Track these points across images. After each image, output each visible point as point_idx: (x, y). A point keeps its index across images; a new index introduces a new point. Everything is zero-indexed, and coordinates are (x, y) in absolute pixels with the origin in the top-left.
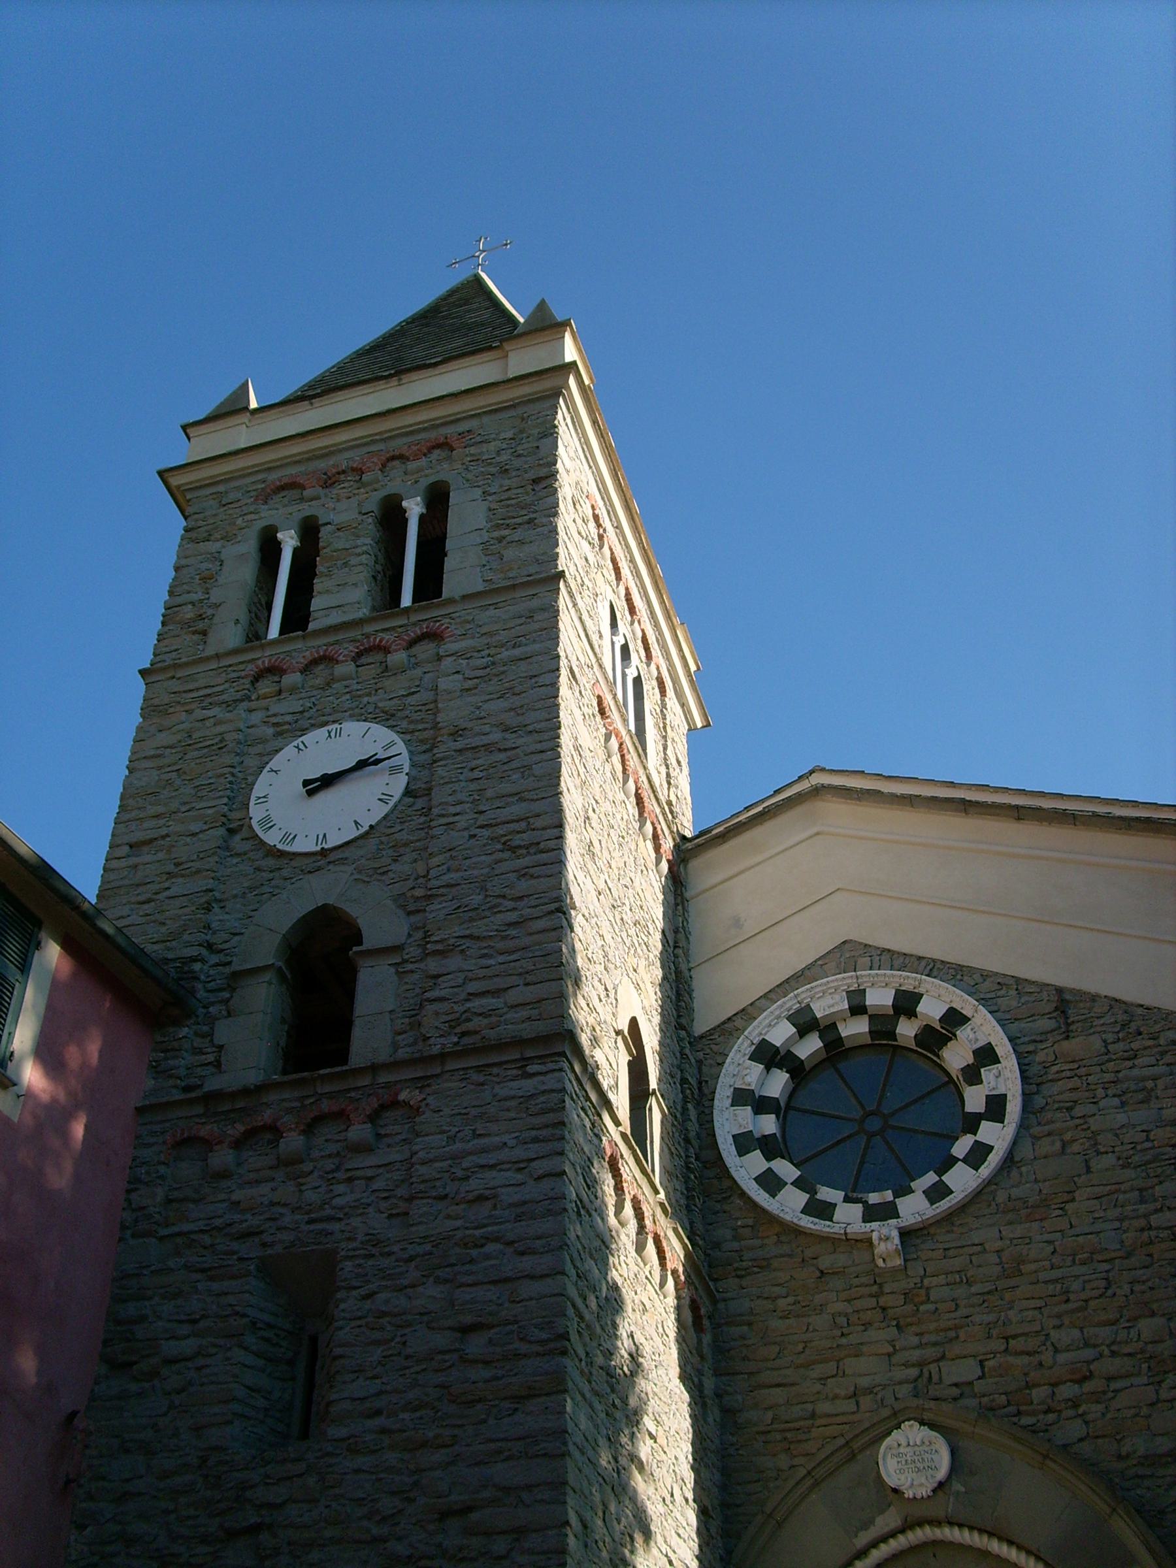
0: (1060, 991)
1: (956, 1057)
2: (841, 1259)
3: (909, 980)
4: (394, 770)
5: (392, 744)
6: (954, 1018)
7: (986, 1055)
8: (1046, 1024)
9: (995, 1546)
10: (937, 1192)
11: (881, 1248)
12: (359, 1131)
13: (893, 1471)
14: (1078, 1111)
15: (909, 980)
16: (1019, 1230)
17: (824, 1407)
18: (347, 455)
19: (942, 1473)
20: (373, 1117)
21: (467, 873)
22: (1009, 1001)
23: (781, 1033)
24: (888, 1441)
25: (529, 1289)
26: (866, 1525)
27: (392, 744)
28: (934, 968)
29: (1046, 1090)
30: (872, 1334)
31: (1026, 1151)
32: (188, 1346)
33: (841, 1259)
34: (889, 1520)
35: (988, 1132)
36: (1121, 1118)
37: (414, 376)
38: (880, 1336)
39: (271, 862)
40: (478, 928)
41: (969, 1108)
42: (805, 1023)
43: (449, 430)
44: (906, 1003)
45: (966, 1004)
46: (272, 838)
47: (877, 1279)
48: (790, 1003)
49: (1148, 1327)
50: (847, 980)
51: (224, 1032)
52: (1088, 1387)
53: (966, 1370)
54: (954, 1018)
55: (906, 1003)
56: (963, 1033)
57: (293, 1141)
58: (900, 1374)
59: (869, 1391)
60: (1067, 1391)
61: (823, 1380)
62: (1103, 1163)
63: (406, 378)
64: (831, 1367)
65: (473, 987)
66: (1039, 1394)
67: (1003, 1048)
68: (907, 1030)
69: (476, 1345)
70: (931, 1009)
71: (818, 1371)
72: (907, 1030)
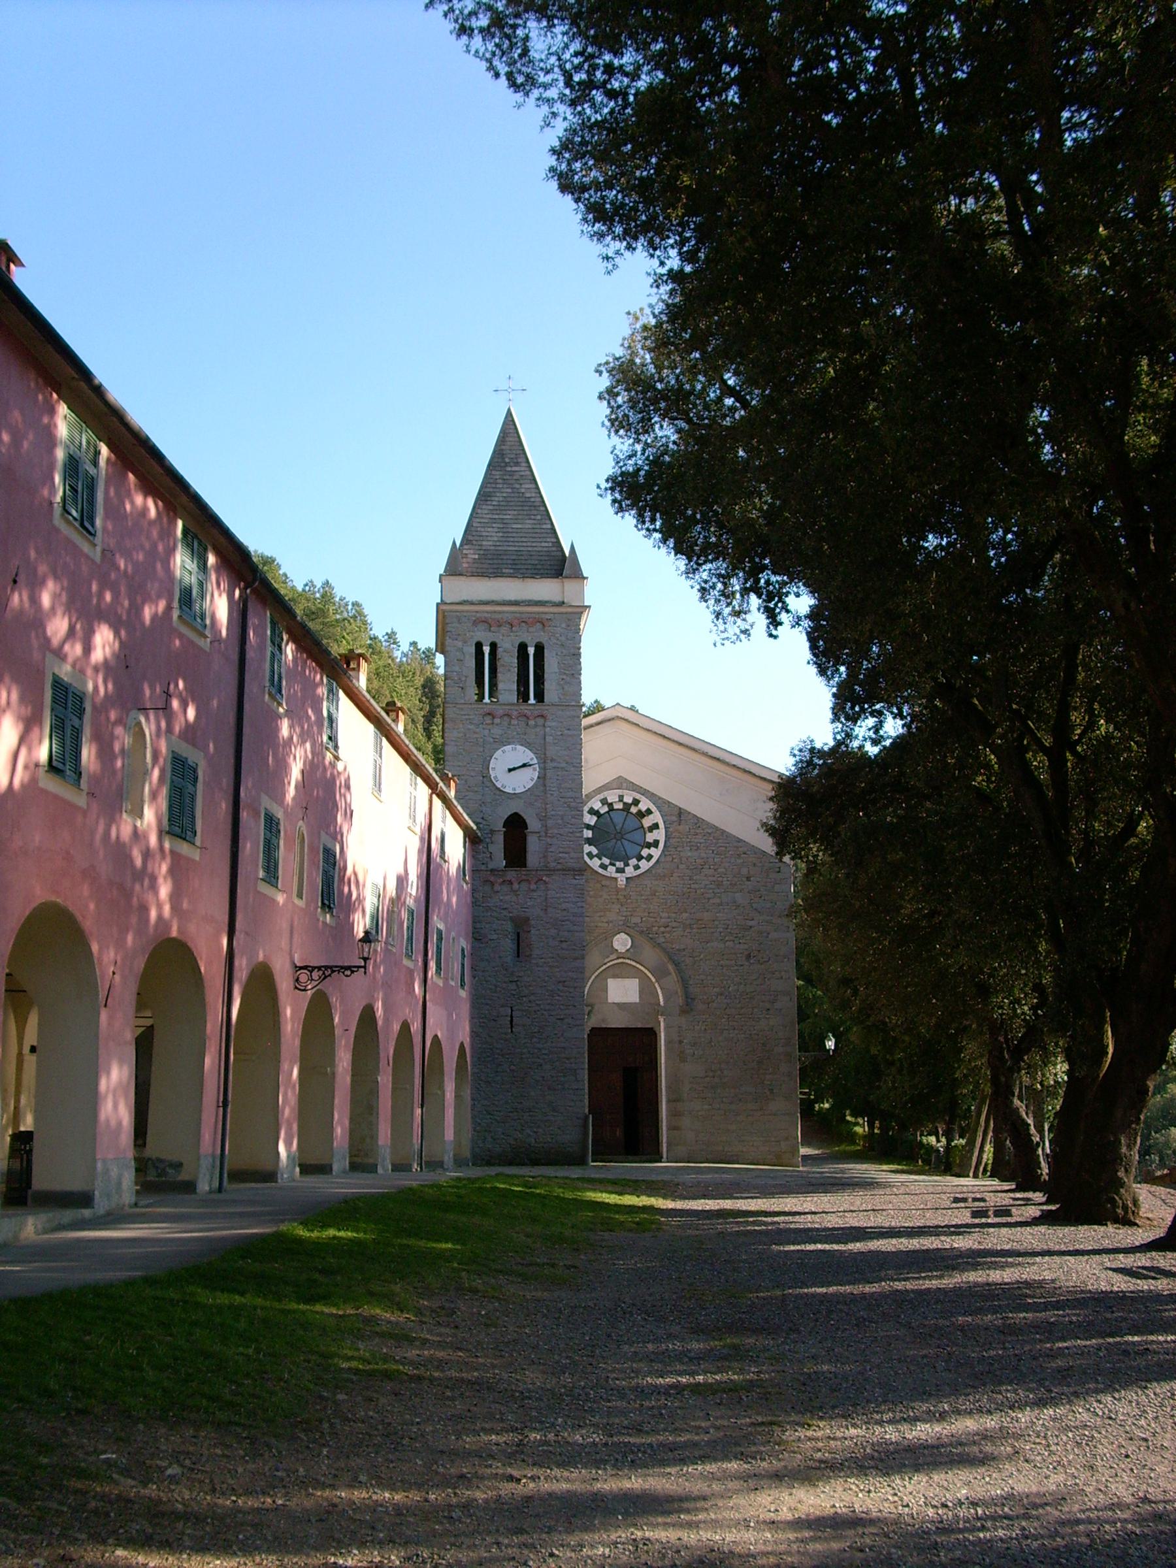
0: (680, 808)
1: (647, 822)
2: (608, 883)
3: (638, 796)
4: (534, 770)
5: (532, 759)
6: (649, 812)
7: (656, 844)
8: (674, 818)
9: (638, 966)
10: (637, 867)
11: (620, 882)
12: (533, 886)
13: (616, 945)
14: (679, 849)
15: (638, 796)
16: (656, 882)
17: (600, 924)
18: (507, 615)
19: (628, 947)
20: (536, 883)
21: (925, 1352)
22: (665, 808)
23: (597, 805)
24: (618, 936)
25: (577, 934)
26: (608, 957)
27: (532, 759)
28: (645, 792)
29: (671, 840)
30: (614, 906)
31: (663, 859)
32: (495, 937)
33: (608, 883)
34: (614, 956)
35: (653, 851)
36: (689, 854)
37: (529, 580)
38: (616, 907)
39: (498, 792)
40: (561, 831)
41: (647, 840)
42: (604, 802)
43: (543, 616)
44: (636, 802)
45: (653, 808)
46: (499, 785)
47: (618, 890)
48: (601, 796)
49: (685, 915)
50: (619, 792)
51: (492, 848)
52: (668, 929)
53: (638, 920)
54: (649, 812)
55: (636, 802)
56: (651, 816)
57: (516, 886)
58: (620, 918)
59: (611, 922)
60: (662, 929)
61: (600, 916)
62: (681, 866)
63: (526, 580)
64: (602, 914)
65: (561, 850)
66: (655, 929)
67: (662, 825)
68: (634, 810)
69: (564, 945)
70: (643, 807)
71: (598, 914)
72: (634, 810)
